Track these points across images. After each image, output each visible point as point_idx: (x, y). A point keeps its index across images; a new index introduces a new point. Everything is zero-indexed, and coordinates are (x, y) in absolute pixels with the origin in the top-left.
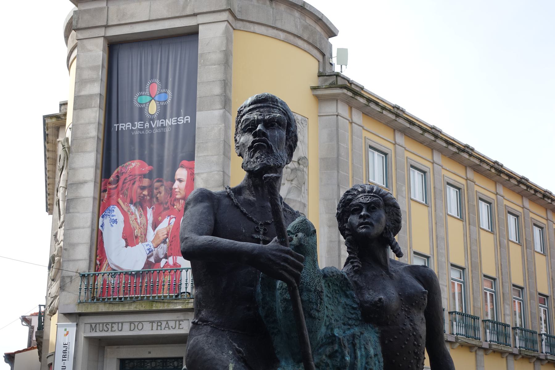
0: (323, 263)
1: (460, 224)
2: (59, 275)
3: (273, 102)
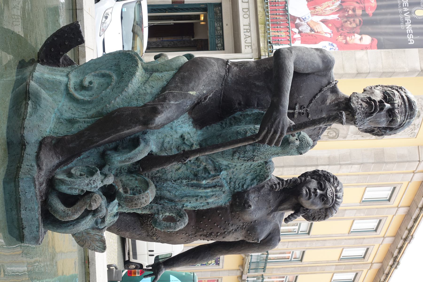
0: (276, 160)
1: (337, 258)
3: (410, 116)
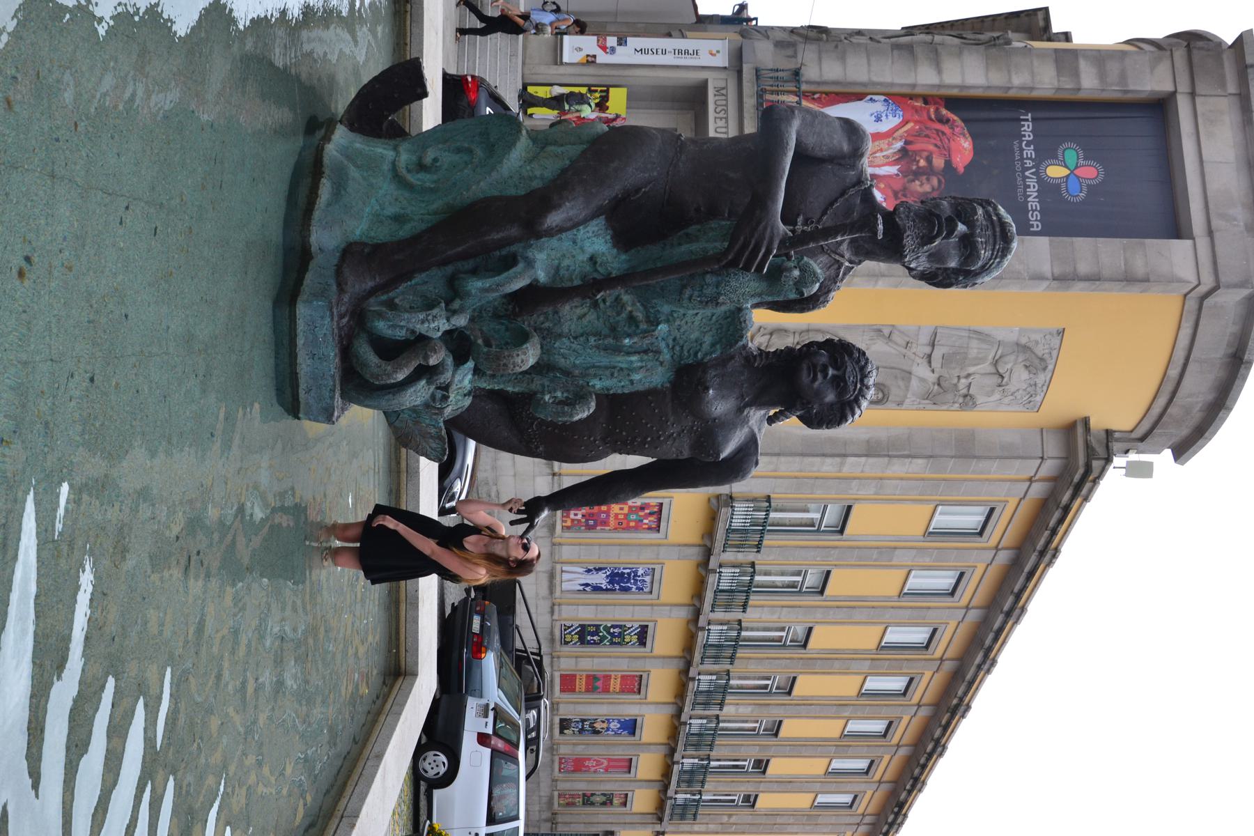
2: (800, 39)
